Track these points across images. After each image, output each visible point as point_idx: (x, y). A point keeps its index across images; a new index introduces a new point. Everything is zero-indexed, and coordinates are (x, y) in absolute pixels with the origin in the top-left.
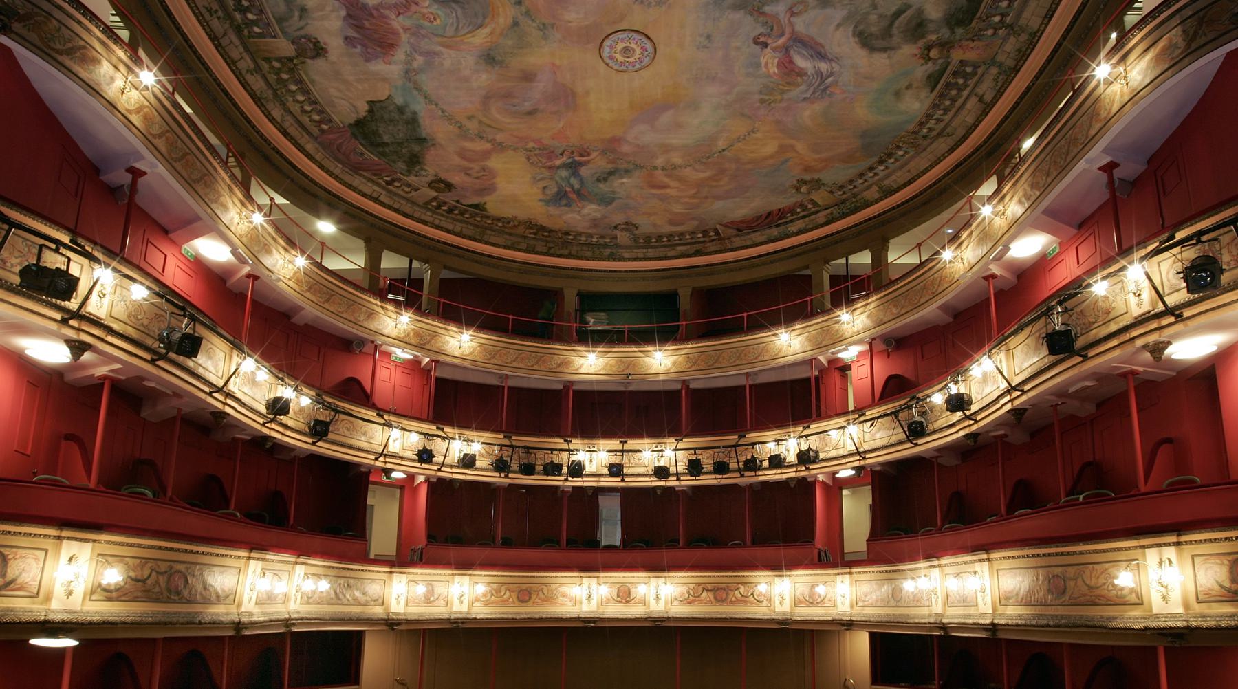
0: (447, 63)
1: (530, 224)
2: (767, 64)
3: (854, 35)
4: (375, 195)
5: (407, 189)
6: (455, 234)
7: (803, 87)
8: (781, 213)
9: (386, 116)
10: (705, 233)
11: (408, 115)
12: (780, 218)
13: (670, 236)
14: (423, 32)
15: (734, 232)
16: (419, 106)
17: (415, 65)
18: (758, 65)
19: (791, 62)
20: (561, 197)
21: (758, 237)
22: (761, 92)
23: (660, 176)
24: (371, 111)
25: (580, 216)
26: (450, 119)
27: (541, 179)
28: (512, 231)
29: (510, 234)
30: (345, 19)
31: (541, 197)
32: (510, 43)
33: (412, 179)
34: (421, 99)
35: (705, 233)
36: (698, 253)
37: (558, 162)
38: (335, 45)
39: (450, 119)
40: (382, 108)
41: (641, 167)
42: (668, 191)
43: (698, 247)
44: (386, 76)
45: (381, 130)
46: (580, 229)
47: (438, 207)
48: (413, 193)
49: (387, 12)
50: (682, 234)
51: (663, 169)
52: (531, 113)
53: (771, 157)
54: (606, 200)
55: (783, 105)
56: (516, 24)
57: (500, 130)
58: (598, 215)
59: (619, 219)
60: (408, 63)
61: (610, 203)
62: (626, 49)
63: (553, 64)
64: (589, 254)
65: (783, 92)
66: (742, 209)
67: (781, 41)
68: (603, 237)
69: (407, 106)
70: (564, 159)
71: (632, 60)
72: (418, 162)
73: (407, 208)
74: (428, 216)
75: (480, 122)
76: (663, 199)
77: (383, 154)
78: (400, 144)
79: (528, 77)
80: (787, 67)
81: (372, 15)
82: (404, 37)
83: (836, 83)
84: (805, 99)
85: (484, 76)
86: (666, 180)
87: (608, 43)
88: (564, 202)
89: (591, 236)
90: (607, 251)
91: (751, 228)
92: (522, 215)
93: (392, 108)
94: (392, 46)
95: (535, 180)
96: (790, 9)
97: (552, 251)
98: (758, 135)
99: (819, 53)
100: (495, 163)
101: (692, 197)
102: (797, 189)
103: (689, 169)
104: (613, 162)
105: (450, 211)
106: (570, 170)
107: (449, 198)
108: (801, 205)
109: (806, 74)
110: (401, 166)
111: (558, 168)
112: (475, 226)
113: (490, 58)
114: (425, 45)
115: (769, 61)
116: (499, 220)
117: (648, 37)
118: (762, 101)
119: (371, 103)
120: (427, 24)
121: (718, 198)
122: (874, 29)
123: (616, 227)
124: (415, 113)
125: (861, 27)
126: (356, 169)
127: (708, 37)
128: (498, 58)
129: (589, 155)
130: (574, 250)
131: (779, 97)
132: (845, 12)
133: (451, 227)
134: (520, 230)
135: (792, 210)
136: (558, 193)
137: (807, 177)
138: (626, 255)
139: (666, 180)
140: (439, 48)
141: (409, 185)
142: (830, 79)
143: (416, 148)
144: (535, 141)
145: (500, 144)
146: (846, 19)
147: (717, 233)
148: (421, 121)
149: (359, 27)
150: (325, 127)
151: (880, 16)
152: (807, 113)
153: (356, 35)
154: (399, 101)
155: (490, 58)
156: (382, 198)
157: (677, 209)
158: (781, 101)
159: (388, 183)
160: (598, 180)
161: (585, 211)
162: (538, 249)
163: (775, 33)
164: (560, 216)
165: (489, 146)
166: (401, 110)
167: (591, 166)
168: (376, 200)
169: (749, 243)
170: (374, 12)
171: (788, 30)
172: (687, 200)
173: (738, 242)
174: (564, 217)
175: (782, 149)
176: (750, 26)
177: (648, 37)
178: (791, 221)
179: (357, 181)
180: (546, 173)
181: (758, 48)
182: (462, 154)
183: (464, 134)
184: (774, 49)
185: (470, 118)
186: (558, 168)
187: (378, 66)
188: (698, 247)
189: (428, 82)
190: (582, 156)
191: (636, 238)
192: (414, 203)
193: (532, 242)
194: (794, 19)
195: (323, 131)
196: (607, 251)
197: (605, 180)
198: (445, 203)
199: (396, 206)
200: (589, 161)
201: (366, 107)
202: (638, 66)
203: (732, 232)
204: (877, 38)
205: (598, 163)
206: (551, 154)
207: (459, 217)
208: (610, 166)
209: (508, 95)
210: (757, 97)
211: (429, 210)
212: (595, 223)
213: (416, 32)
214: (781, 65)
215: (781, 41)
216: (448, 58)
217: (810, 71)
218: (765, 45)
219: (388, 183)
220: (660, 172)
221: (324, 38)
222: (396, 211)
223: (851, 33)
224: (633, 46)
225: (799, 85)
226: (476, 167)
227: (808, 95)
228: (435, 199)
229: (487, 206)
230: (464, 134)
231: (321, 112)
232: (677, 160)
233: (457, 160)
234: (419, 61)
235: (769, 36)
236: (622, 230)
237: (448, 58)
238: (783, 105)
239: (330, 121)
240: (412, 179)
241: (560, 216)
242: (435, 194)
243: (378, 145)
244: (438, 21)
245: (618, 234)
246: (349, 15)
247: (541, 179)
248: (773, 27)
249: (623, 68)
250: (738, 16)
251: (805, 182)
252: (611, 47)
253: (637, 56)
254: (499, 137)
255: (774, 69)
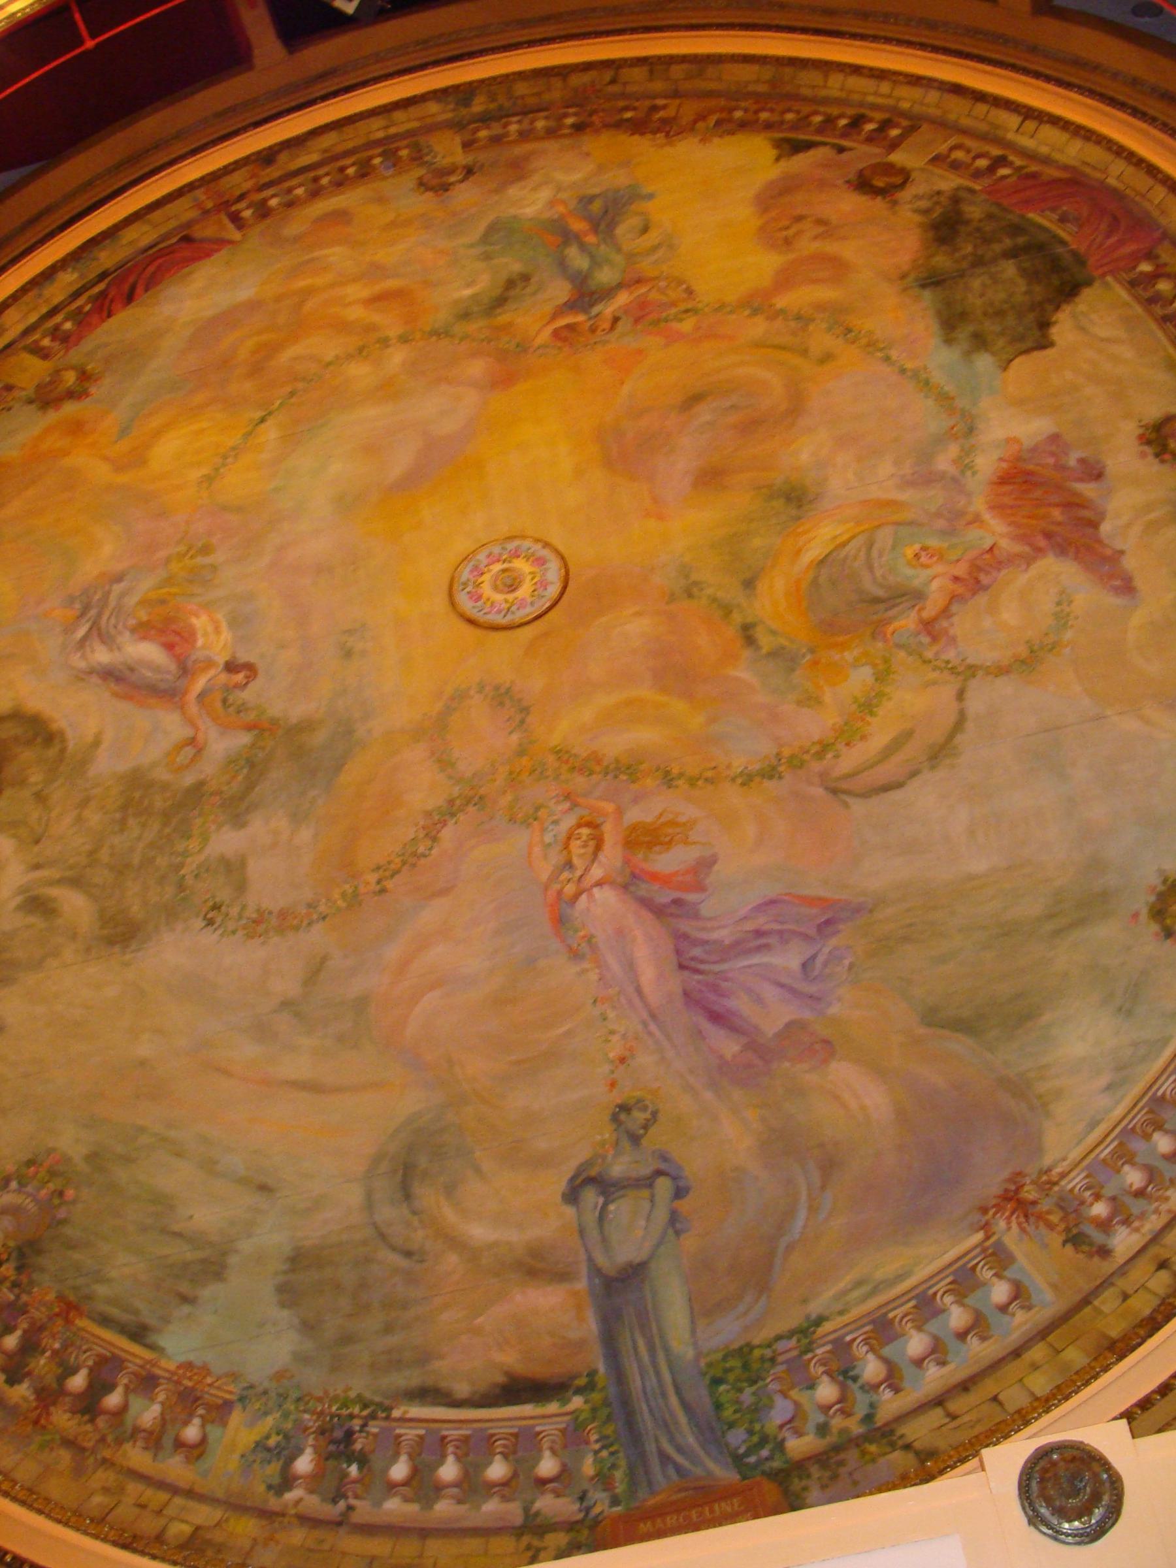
0: (886, 468)
1: (669, 129)
2: (217, 630)
3: (61, 733)
4: (1030, 125)
5: (959, 155)
6: (841, 67)
7: (132, 601)
8: (104, 307)
9: (1011, 320)
10: (263, 212)
11: (964, 333)
12: (103, 294)
13: (340, 184)
14: (941, 523)
15: (198, 232)
16: (940, 358)
17: (953, 450)
18: (235, 622)
19: (169, 647)
20: (605, 213)
21: (141, 236)
22: (214, 568)
23: (389, 322)
24: (1044, 325)
25: (555, 180)
26: (871, 346)
27: (655, 249)
28: (712, 103)
29: (710, 94)
30: (1102, 516)
31: (649, 206)
32: (757, 542)
33: (948, 182)
34: (938, 377)
35: (263, 212)
36: (267, 157)
37: (623, 298)
38: (1124, 457)
39: (871, 346)
40: (1022, 338)
41: (436, 333)
42: (366, 293)
43: (273, 172)
44: (1010, 417)
45: (1022, 285)
46: (552, 145)
47: (885, 125)
48: (943, 148)
49: (1018, 548)
50: (315, 194)
51: (385, 342)
52: (694, 399)
53: (158, 434)
54: (500, 233)
55: (162, 554)
56: (749, 584)
57: (758, 345)
58: (513, 191)
59: (465, 195)
60: (967, 452)
61: (492, 229)
62: (512, 586)
63: (661, 517)
64: (521, 89)
65: (169, 581)
66: (190, 301)
67: (200, 683)
68: (496, 140)
69: (968, 354)
70: (608, 309)
71: (497, 567)
72: (935, 226)
73: (957, 109)
74: (907, 98)
75: (804, 353)
76: (377, 271)
77: (1016, 229)
78: (978, 262)
79: (711, 478)
80: (171, 633)
81: (1048, 535)
82: (979, 504)
83: (68, 630)
84: (119, 579)
85: (805, 457)
86: (376, 318)
87: (553, 591)
88: (597, 206)
89: (524, 136)
90: (479, 105)
91: (169, 251)
92: (687, 150)
93: (1001, 343)
94: (1004, 480)
95: (669, 244)
96: (200, 751)
97: (608, 75)
98: (195, 474)
99: (119, 679)
100: (764, 264)
101: (310, 292)
102: (85, 376)
103: (330, 356)
104: (506, 328)
105: (857, 122)
106: (594, 289)
107: (863, 154)
108: (66, 339)
109: (133, 630)
110: (974, 211)
111: (620, 286)
112: (796, 97)
113: (796, 499)
114: (936, 497)
115: (214, 639)
116: (743, 126)
117: (471, 622)
118: (206, 550)
119: (1045, 344)
120: (933, 542)
121: (253, 306)
122: (27, 755)
123: (469, 171)
124: (949, 341)
125: (52, 752)
126: (1074, 183)
127: (348, 654)
128: (778, 504)
129: (556, 334)
130: (556, 92)
131: (175, 566)
132: (92, 772)
133: (854, 82)
134: (689, 109)
135: (84, 322)
136: (612, 226)
137: (70, 408)
138: (433, 107)
139: (376, 318)
140: (905, 496)
141: (955, 166)
142: (81, 632)
143: (942, 261)
144: (681, 336)
145: (756, 312)
146: (83, 763)
147: (236, 219)
148: (935, 326)
149: (1074, 504)
150: (1145, 267)
151: (22, 782)
152: (108, 549)
153: (1080, 487)
154: (984, 362)
155: (796, 499)
156: (1013, 120)
157: (336, 255)
158: (168, 561)
159: (1001, 161)
160: (526, 278)
161: (545, 194)
162: (638, 73)
163: (218, 697)
164: (601, 168)
165: (781, 302)
166: (980, 342)
167: (549, 308)
168: (1029, 113)
169: (157, 215)
170: (1042, 542)
171: (193, 709)
172: (319, 281)
173: (183, 211)
174: (589, 167)
175: (137, 458)
176: (271, 696)
177: (471, 622)
178: (76, 295)
179: (1073, 151)
180: (646, 266)
181: (243, 657)
182: (837, 269)
183: (840, 320)
184: (209, 663)
185: (827, 358)
186: (620, 286)
187: (1030, 429)
188: (273, 172)
189: (925, 416)
190: (570, 327)
191: (418, 157)
192: (942, 125)
193: (658, 86)
194: (188, 732)
195: (1149, 256)
196: (479, 105)
197: (510, 284)
198: (870, 139)
199: (982, 108)
200: (555, 316)
201: (1055, 332)
202: (482, 557)
203: (205, 231)
204: (16, 739)
205: (532, 318)
206: (641, 313)
207: (835, 111)
208: (503, 318)
209: (750, 426)
210: (218, 557)
211: (903, 114)
212: (518, 170)
213: (956, 520)
214: (188, 636)
215: (200, 683)
216: (884, 479)
217: (125, 639)
218: (231, 667)
219: (1001, 161)
220: (392, 333)
221: (1150, 467)
222: (980, 97)
223: (70, 734)
224: (498, 597)
225: (143, 602)
226: (808, 246)
227: (117, 588)
228: (894, 145)
229: (772, 153)
230: (840, 320)
231: (1153, 300)
232: (360, 372)
233: (847, 250)
234: (944, 462)
235: (228, 689)
236: (451, 171)
237: (884, 479)
238: (162, 554)
239: (1133, 284)
240: (948, 182)
241: (601, 168)
242: (897, 157)
243: (1026, 249)
244: (909, 552)
245: (460, 158)
246: (1094, 525)
247: (655, 249)
248: (226, 707)
249: (511, 546)
250: (298, 711)
251: (71, 395)
252: (544, 584)
253: (486, 578)
254: (758, 328)
255: (200, 622)
